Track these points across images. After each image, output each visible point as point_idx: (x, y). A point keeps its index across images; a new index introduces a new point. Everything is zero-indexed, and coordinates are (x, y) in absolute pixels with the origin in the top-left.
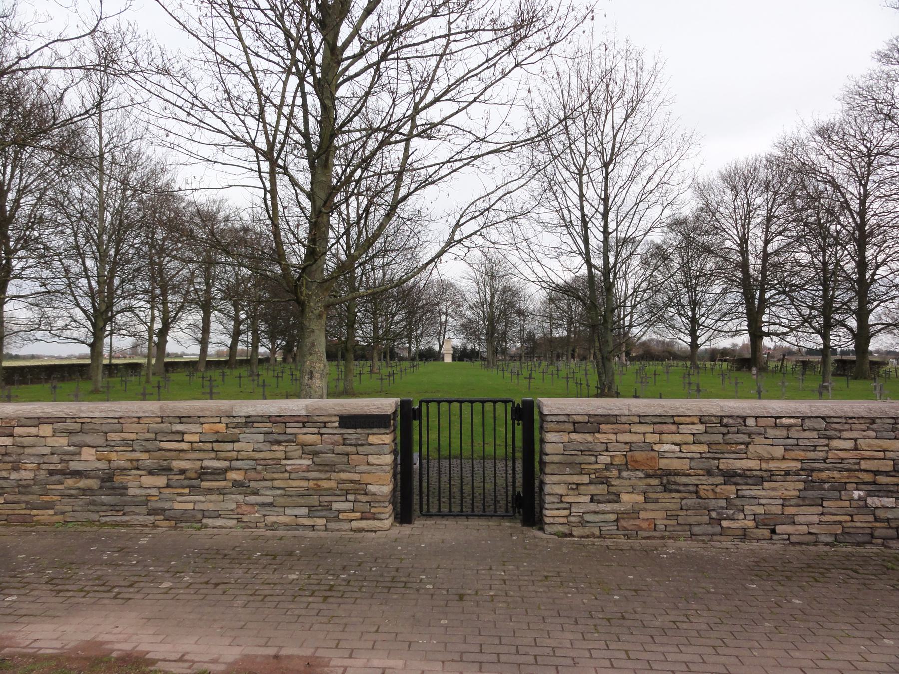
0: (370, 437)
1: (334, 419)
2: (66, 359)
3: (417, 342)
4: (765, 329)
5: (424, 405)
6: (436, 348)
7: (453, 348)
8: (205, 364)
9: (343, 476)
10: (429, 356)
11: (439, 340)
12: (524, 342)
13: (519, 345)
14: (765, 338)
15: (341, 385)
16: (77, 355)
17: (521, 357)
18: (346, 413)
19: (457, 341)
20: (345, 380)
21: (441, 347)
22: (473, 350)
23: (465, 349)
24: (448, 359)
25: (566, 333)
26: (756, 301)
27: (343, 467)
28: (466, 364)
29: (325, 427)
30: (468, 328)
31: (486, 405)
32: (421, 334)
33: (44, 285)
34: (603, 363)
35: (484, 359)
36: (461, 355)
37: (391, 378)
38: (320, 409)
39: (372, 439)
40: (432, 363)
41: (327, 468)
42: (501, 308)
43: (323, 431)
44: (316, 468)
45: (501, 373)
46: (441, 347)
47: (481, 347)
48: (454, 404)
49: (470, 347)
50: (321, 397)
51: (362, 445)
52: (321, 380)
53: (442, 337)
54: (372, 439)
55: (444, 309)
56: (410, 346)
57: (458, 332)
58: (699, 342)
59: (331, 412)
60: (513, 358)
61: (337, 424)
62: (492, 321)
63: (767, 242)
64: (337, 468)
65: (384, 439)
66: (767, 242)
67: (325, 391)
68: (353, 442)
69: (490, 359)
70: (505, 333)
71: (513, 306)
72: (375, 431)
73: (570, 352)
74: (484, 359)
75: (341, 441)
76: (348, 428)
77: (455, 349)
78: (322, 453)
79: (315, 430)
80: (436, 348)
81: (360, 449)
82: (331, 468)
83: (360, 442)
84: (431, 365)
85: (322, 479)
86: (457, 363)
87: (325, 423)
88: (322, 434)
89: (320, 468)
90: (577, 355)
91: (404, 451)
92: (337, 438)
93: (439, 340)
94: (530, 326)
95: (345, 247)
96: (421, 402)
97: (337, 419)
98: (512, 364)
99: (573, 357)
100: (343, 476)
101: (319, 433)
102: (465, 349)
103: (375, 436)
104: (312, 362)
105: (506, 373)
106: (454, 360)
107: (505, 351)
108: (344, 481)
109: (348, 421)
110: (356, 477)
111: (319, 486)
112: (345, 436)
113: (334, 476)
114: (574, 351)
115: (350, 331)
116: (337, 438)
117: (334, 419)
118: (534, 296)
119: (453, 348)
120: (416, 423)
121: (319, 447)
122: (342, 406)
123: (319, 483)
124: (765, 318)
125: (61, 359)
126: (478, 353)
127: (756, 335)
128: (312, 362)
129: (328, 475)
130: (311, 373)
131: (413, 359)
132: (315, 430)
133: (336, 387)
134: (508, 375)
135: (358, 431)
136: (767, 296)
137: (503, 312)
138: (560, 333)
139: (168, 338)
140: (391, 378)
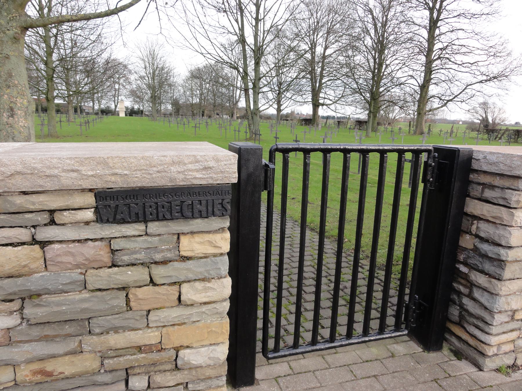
0: (185, 241)
1: (79, 200)
3: (99, 101)
4: (321, 101)
5: (279, 156)
6: (113, 107)
9: (116, 340)
11: (114, 101)
14: (320, 107)
15: (46, 129)
18: (118, 183)
19: (128, 103)
20: (49, 125)
21: (116, 106)
23: (133, 108)
24: (122, 115)
25: (198, 100)
26: (318, 85)
27: (116, 320)
28: (134, 118)
29: (52, 222)
31: (291, 155)
32: (102, 96)
34: (252, 117)
36: (131, 113)
37: (87, 124)
38: (33, 173)
39: (190, 245)
41: (68, 329)
42: (158, 81)
43: (44, 234)
44: (36, 332)
46: (116, 106)
47: (146, 107)
48: (352, 154)
49: (136, 107)
50: (28, 139)
51: (164, 262)
52: (26, 119)
53: (116, 99)
54: (190, 245)
56: (94, 104)
58: (282, 108)
59: (68, 180)
61: (89, 215)
63: (326, 48)
64: (97, 325)
65: (211, 241)
66: (326, 48)
67: (33, 132)
68: (141, 256)
72: (198, 224)
73: (201, 112)
75: (106, 258)
76: (123, 221)
77: (127, 108)
78: (49, 293)
79: (24, 235)
81: (159, 272)
82: (83, 324)
83: (158, 257)
85: (54, 356)
86: (128, 117)
87: (52, 212)
88: (43, 244)
89: (48, 331)
90: (205, 114)
91: (243, 261)
92: (90, 250)
93: (114, 101)
94: (176, 95)
95: (38, 8)
96: (272, 154)
97: (90, 199)
99: (203, 115)
100: (116, 340)
101: (34, 241)
103: (198, 238)
104: (11, 97)
106: (126, 115)
108: (119, 352)
109: (119, 205)
110: (150, 337)
111: (49, 374)
112: (115, 245)
113: (91, 342)
115: (50, 84)
116: (90, 250)
117: (79, 200)
120: (264, 195)
121: (36, 281)
122: (104, 163)
123: (49, 366)
124: (322, 95)
126: (142, 111)
127: (316, 105)
128: (11, 97)
129: (73, 344)
130: (12, 109)
131: (97, 114)
132: (24, 235)
133: (41, 130)
135: (154, 227)
136: (323, 81)
140: (87, 124)
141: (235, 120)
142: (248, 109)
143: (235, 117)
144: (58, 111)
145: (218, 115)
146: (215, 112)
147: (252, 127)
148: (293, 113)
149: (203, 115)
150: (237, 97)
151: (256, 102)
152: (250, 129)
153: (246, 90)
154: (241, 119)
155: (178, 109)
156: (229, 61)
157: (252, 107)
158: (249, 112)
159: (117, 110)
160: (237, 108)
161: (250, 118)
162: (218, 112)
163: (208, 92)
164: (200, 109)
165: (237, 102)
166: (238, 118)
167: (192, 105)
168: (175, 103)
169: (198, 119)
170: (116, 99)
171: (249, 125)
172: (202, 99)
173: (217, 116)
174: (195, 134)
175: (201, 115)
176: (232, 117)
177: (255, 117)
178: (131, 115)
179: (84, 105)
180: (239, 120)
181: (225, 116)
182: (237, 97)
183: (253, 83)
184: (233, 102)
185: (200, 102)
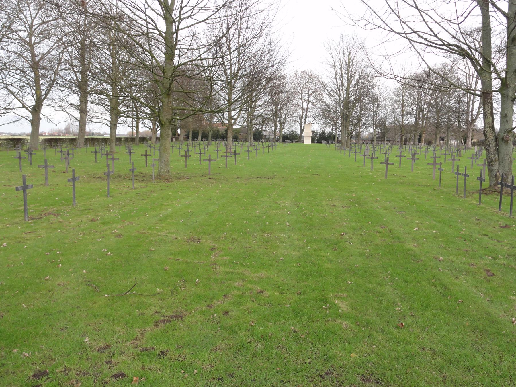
2: (19, 135)
6: (299, 132)
7: (313, 132)
8: (83, 140)
10: (293, 138)
12: (376, 127)
13: (371, 130)
16: (7, 132)
17: (372, 141)
19: (317, 126)
21: (302, 131)
22: (331, 133)
23: (323, 133)
24: (308, 141)
25: (414, 120)
28: (324, 145)
30: (326, 114)
33: (28, 81)
34: (497, 145)
35: (339, 142)
36: (320, 139)
40: (294, 144)
45: (353, 155)
46: (302, 131)
49: (328, 130)
53: (303, 121)
55: (306, 98)
57: (317, 117)
60: (366, 141)
62: (347, 106)
69: (344, 141)
70: (359, 119)
71: (368, 93)
73: (417, 137)
74: (339, 142)
80: (299, 132)
84: (291, 146)
90: (423, 139)
94: (382, 114)
98: (364, 147)
99: (419, 141)
102: (323, 133)
105: (358, 155)
106: (313, 141)
107: (358, 136)
114: (420, 136)
118: (386, 88)
119: (313, 132)
125: (14, 135)
134: (360, 157)
137: (358, 99)
138: (409, 120)
139: (41, 116)
141: (468, 148)
142: (489, 130)
143: (469, 143)
144: (236, 138)
145: (443, 140)
146: (438, 136)
147: (496, 167)
148: (41, 119)
149: (419, 141)
150: (475, 113)
151: (505, 117)
152: (490, 170)
153: (486, 95)
154: (479, 145)
155: (385, 134)
156: (453, 41)
157: (497, 126)
158: (491, 137)
159: (303, 135)
160: (474, 130)
161: (493, 148)
162: (443, 135)
163: (429, 107)
164: (415, 131)
165: (473, 120)
166: (474, 144)
167: (403, 126)
168: (381, 124)
169: (411, 146)
170: (303, 121)
171: (490, 163)
172: (419, 118)
173: (441, 142)
174: (386, 176)
175: (417, 140)
176: (465, 142)
177: (502, 146)
178: (319, 142)
179: (266, 130)
180: (476, 148)
181: (453, 142)
182: (475, 113)
183: (502, 79)
184: (467, 120)
185: (417, 122)
